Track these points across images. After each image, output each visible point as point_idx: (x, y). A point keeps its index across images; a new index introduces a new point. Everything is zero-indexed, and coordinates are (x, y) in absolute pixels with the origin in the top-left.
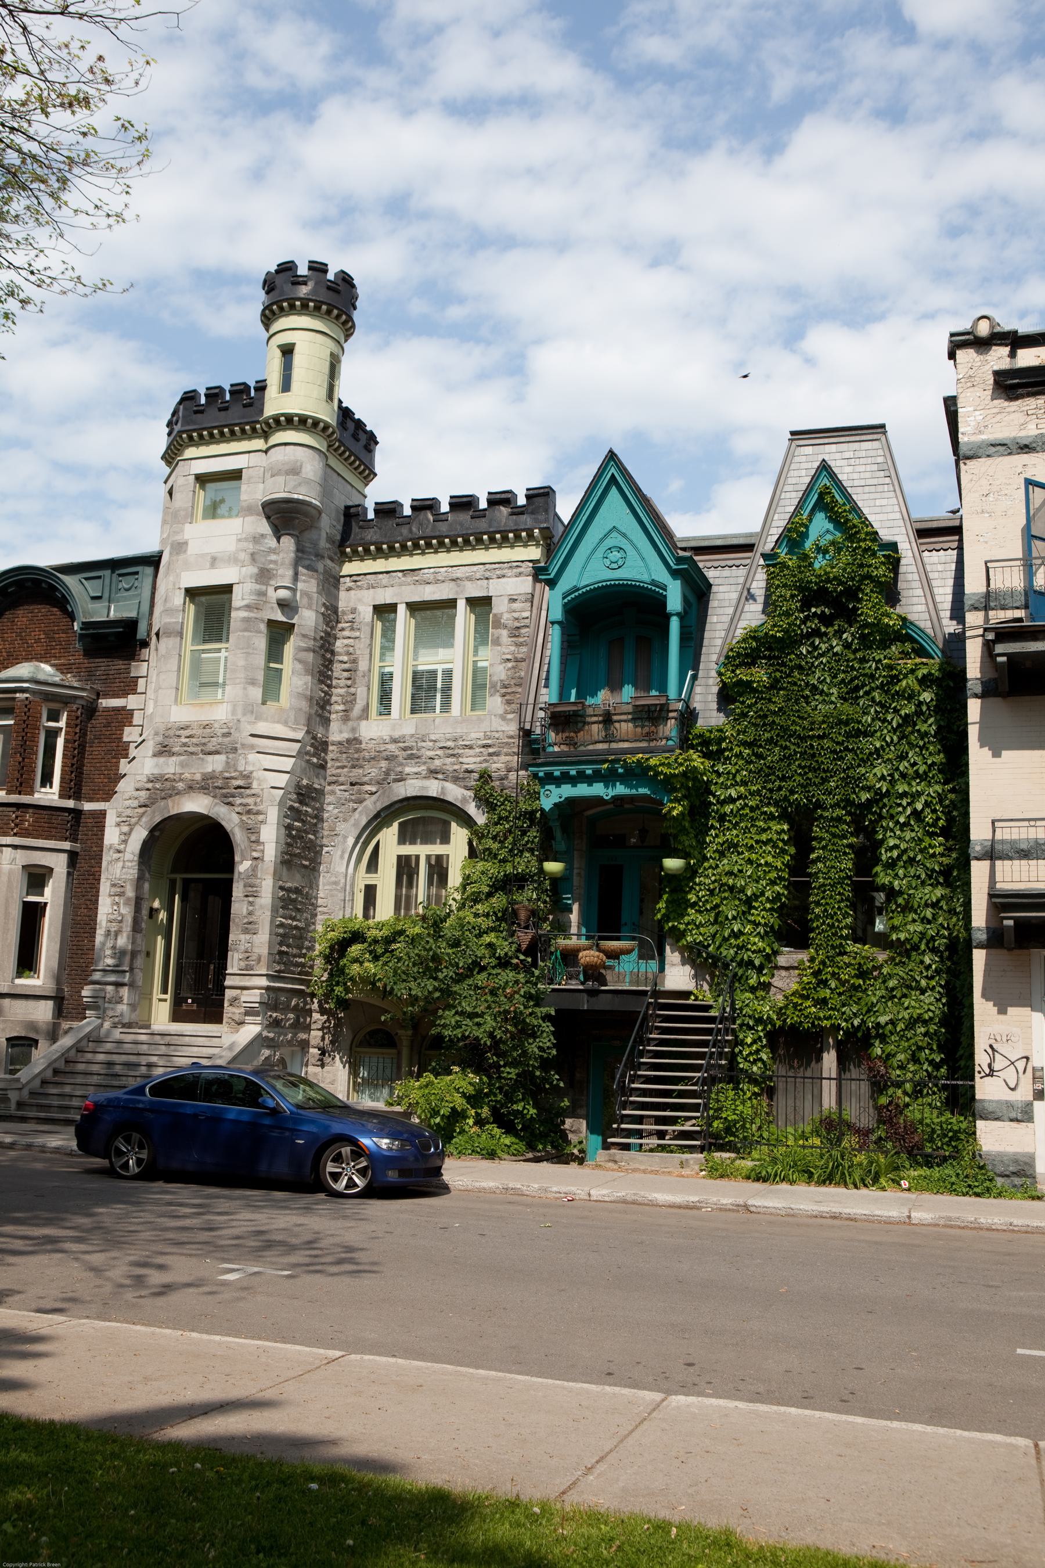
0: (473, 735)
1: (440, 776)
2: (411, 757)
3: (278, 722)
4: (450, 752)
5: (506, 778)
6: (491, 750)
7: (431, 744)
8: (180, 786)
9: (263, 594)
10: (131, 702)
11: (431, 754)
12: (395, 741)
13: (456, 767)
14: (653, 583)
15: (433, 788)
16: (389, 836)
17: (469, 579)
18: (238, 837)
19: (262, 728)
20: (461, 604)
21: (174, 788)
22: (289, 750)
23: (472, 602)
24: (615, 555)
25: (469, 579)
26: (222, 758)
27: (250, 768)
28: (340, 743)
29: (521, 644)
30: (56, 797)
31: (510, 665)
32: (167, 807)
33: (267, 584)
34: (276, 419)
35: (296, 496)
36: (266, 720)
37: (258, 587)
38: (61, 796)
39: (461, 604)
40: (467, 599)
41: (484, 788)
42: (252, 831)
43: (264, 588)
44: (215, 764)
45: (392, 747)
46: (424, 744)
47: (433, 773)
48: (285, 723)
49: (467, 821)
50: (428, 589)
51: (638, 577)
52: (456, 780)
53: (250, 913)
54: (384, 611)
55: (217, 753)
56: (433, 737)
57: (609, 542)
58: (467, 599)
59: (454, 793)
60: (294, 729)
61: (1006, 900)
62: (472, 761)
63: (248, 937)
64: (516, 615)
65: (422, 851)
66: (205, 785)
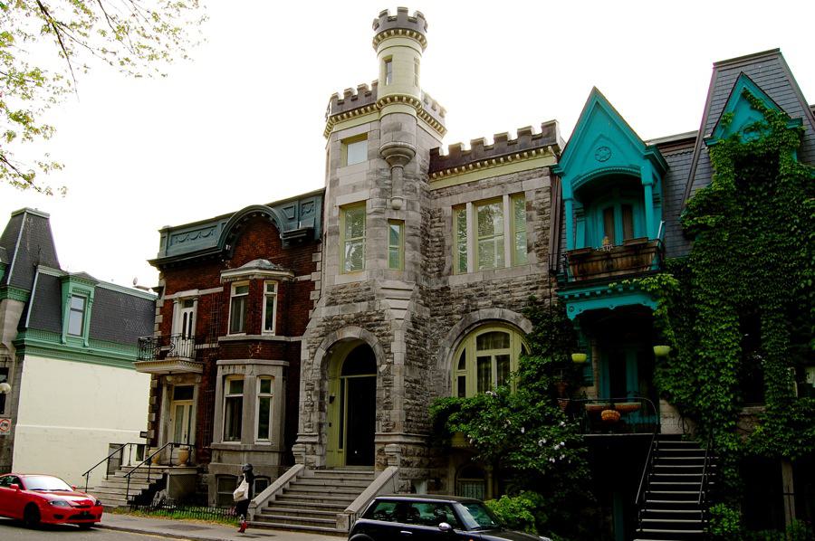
0: (520, 278)
1: (500, 306)
2: (481, 295)
4: (506, 290)
5: (543, 303)
6: (531, 287)
10: (314, 277)
11: (494, 292)
12: (470, 286)
13: (510, 299)
14: (631, 166)
15: (496, 313)
16: (471, 344)
17: (510, 182)
18: (378, 350)
19: (388, 284)
20: (506, 198)
21: (338, 324)
24: (603, 153)
25: (510, 182)
26: (366, 303)
29: (546, 219)
30: (274, 335)
31: (539, 232)
32: (335, 336)
39: (506, 198)
41: (533, 309)
42: (386, 346)
44: (362, 308)
45: (469, 290)
47: (496, 304)
49: (521, 332)
50: (484, 192)
51: (619, 164)
52: (510, 307)
55: (364, 301)
56: (494, 282)
57: (599, 145)
59: (510, 315)
62: (520, 294)
63: (387, 411)
64: (541, 201)
66: (357, 321)
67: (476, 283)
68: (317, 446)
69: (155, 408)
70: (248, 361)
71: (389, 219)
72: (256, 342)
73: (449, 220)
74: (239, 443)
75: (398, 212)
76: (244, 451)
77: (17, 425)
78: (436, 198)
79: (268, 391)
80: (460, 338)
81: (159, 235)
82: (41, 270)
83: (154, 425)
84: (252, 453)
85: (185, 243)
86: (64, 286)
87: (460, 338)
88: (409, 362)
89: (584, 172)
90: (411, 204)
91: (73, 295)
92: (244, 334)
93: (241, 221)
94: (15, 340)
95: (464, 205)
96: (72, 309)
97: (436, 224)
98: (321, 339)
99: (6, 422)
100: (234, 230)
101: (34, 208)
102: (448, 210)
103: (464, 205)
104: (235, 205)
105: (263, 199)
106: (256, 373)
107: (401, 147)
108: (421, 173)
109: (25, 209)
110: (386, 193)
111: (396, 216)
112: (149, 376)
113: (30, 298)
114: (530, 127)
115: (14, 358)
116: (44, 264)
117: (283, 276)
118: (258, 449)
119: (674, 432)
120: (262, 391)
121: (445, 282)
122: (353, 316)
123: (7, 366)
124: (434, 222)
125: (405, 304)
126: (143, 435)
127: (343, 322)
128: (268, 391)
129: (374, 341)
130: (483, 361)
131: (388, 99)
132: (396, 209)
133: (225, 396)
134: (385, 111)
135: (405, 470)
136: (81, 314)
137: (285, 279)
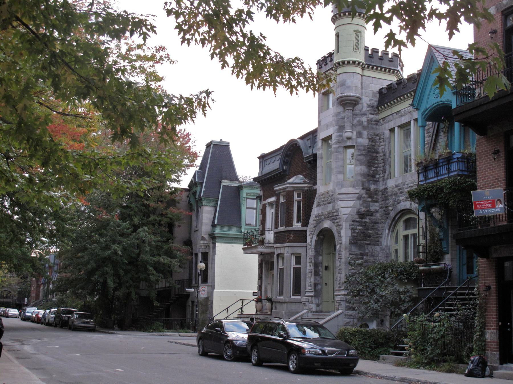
3: (350, 187)
7: (406, 186)
8: (323, 217)
9: (341, 136)
16: (401, 226)
18: (336, 235)
19: (343, 190)
21: (321, 219)
22: (353, 198)
23: (401, 127)
27: (338, 207)
28: (382, 190)
30: (301, 226)
33: (343, 132)
34: (339, 63)
35: (344, 95)
36: (346, 187)
37: (339, 134)
38: (302, 226)
40: (399, 126)
42: (339, 233)
43: (341, 133)
45: (396, 189)
46: (404, 186)
48: (354, 187)
50: (403, 118)
53: (340, 265)
54: (392, 130)
58: (399, 126)
60: (357, 189)
61: (194, 264)
65: (409, 232)
67: (399, 184)
68: (313, 298)
69: (260, 278)
70: (285, 245)
71: (344, 146)
72: (290, 232)
73: (387, 141)
74: (299, 297)
75: (351, 140)
76: (285, 302)
77: (215, 290)
78: (382, 125)
79: (300, 264)
80: (394, 223)
81: (258, 160)
82: (225, 183)
83: (260, 287)
84: (289, 304)
85: (270, 165)
86: (241, 192)
87: (394, 223)
88: (355, 241)
89: (428, 107)
90: (360, 135)
91: (247, 198)
92: (284, 227)
93: (289, 150)
94: (210, 233)
95: (409, 123)
96: (247, 208)
97: (382, 144)
98: (314, 229)
99: (204, 289)
100: (287, 156)
101: (218, 140)
102: (387, 132)
103: (409, 123)
104: (284, 141)
105: (296, 135)
106: (290, 252)
107: (345, 96)
108: (368, 109)
109: (211, 142)
110: (341, 128)
111: (349, 143)
112: (257, 255)
113: (217, 204)
114: (228, 143)
115: (211, 245)
116: (226, 179)
117: (305, 187)
118: (292, 301)
119: (199, 268)
120: (296, 263)
121: (386, 184)
122: (326, 213)
123: (207, 251)
124: (381, 142)
125: (351, 204)
126: (254, 294)
127: (323, 217)
128: (300, 264)
129: (334, 230)
130: (406, 237)
131: (341, 63)
132: (349, 138)
133: (279, 267)
134: (339, 71)
135: (350, 312)
136: (255, 210)
137: (306, 189)
